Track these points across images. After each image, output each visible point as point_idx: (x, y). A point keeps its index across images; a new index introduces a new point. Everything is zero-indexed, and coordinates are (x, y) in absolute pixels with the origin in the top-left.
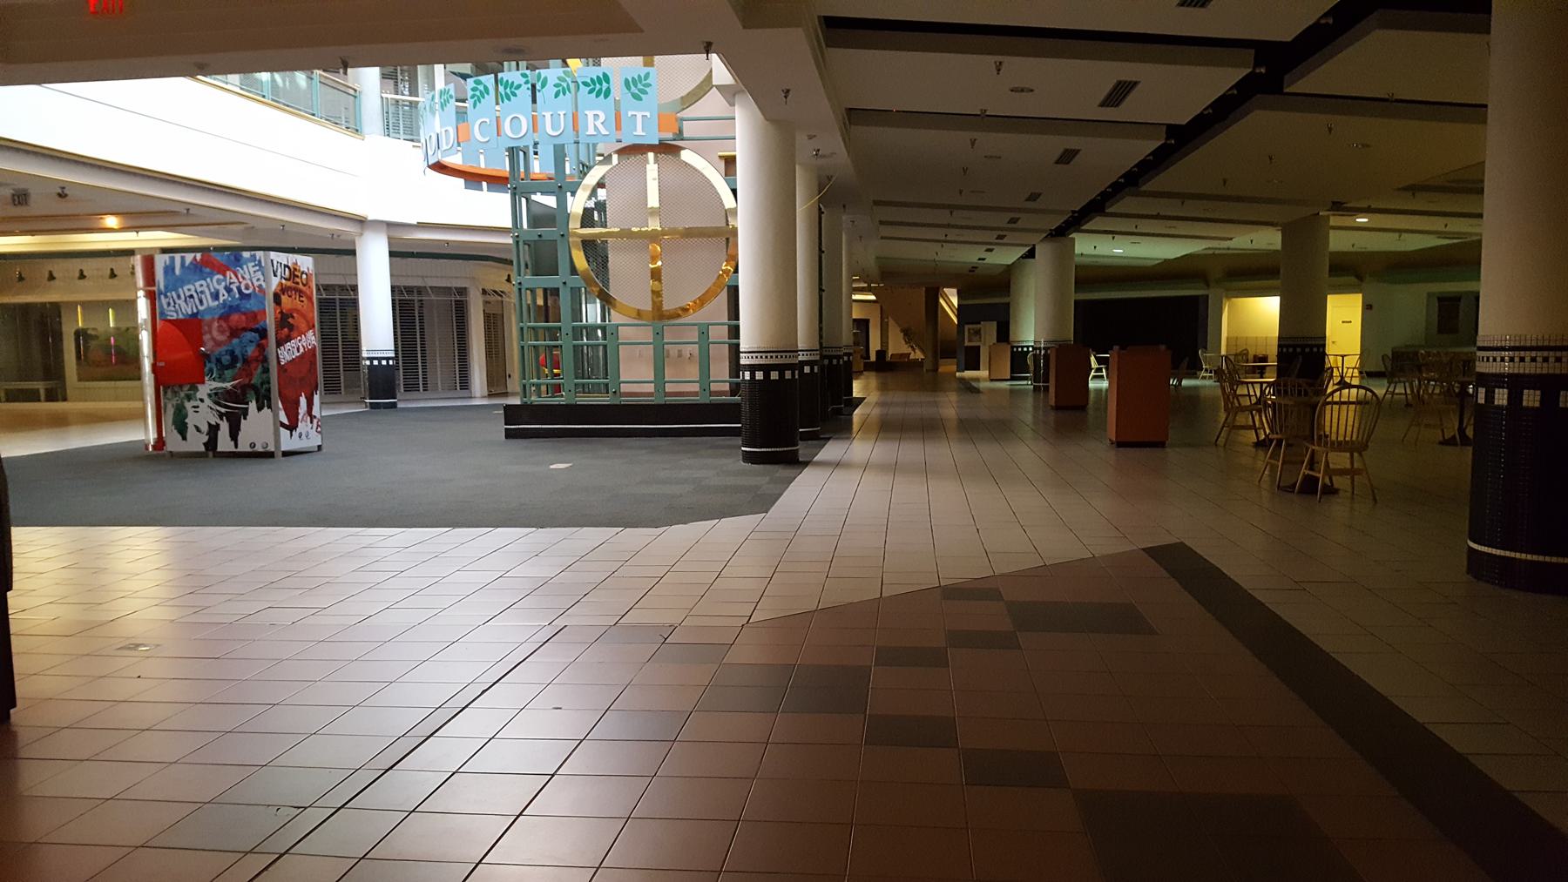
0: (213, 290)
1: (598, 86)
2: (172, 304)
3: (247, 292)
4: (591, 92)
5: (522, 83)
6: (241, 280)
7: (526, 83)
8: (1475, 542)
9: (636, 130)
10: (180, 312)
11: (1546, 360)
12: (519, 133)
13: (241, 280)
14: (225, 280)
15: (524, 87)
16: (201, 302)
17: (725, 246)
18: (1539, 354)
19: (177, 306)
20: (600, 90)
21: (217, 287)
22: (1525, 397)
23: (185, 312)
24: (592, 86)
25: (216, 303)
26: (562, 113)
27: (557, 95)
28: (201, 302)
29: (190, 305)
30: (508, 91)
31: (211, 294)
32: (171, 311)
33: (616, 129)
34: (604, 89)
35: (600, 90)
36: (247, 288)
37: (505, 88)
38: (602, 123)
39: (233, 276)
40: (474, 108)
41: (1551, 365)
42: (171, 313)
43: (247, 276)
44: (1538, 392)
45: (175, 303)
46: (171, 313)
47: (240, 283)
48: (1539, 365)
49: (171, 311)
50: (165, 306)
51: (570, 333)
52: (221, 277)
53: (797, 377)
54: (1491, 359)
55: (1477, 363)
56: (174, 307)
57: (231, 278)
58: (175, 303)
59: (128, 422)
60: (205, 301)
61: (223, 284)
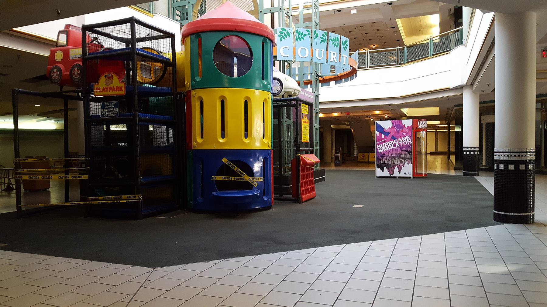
0: (394, 144)
2: (380, 148)
7: (309, 34)
8: (495, 210)
11: (511, 156)
13: (403, 140)
14: (398, 141)
15: (308, 36)
16: (390, 147)
18: (513, 154)
19: (382, 148)
22: (509, 167)
26: (323, 50)
27: (321, 42)
28: (390, 147)
30: (300, 36)
31: (393, 145)
33: (187, 13)
34: (337, 43)
37: (299, 35)
39: (400, 139)
41: (513, 157)
42: (380, 150)
43: (406, 140)
44: (513, 165)
45: (381, 147)
46: (380, 150)
48: (517, 157)
50: (378, 148)
53: (495, 165)
54: (498, 156)
55: (495, 157)
57: (400, 140)
58: (381, 147)
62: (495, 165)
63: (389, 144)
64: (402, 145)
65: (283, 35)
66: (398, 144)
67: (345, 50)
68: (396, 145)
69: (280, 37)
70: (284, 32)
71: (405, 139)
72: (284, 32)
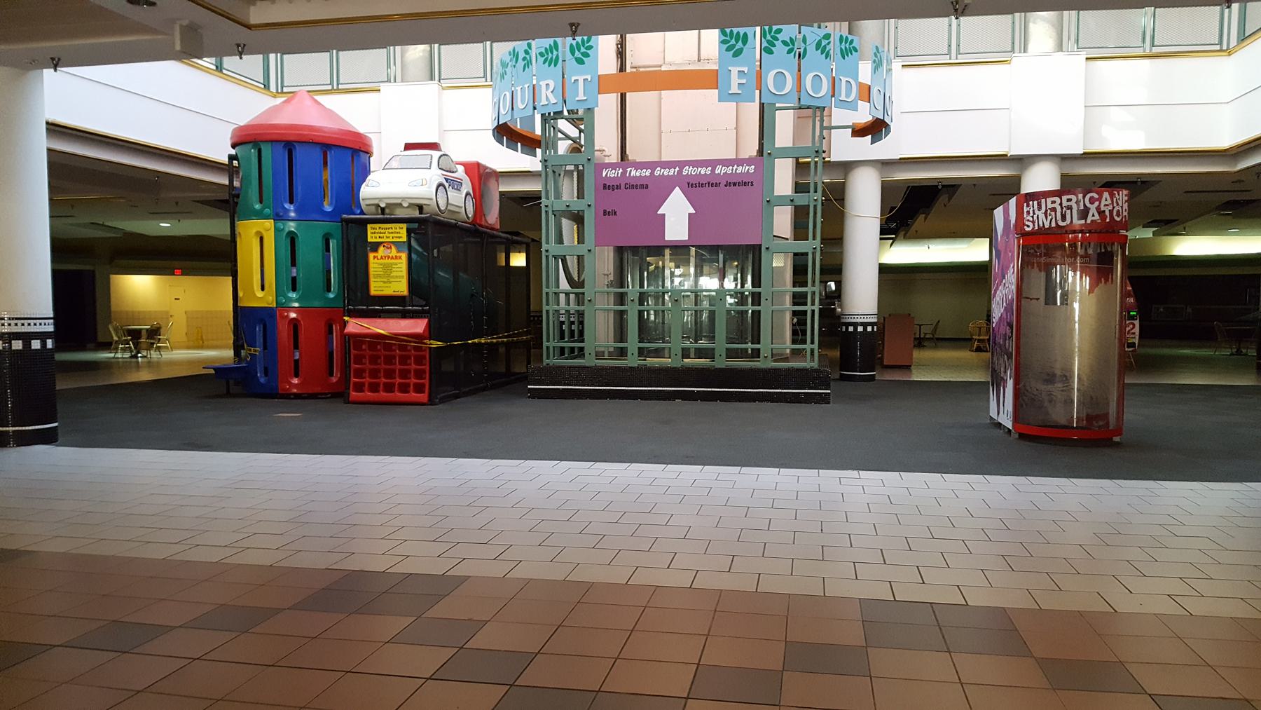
0: (1082, 207)
1: (733, 42)
3: (1118, 219)
4: (789, 52)
5: (780, 42)
6: (1115, 205)
9: (840, 96)
10: (1036, 224)
12: (782, 90)
13: (1115, 205)
14: (1099, 200)
17: (506, 231)
19: (1035, 217)
20: (734, 46)
21: (1088, 204)
23: (1041, 225)
24: (791, 46)
25: (1083, 222)
28: (1064, 218)
29: (1049, 218)
32: (1028, 220)
34: (843, 43)
35: (734, 46)
36: (1118, 215)
38: (552, 92)
40: (524, 71)
45: (1034, 214)
47: (1114, 207)
49: (1028, 220)
51: (763, 300)
52: (1096, 196)
53: (875, 330)
56: (1033, 217)
58: (1034, 214)
59: (842, 292)
60: (1068, 217)
61: (1097, 203)
62: (875, 330)
63: (1065, 203)
64: (1108, 220)
65: (583, 50)
66: (1096, 214)
67: (844, 58)
68: (1090, 214)
69: (589, 44)
70: (580, 56)
71: (1121, 199)
72: (580, 56)
